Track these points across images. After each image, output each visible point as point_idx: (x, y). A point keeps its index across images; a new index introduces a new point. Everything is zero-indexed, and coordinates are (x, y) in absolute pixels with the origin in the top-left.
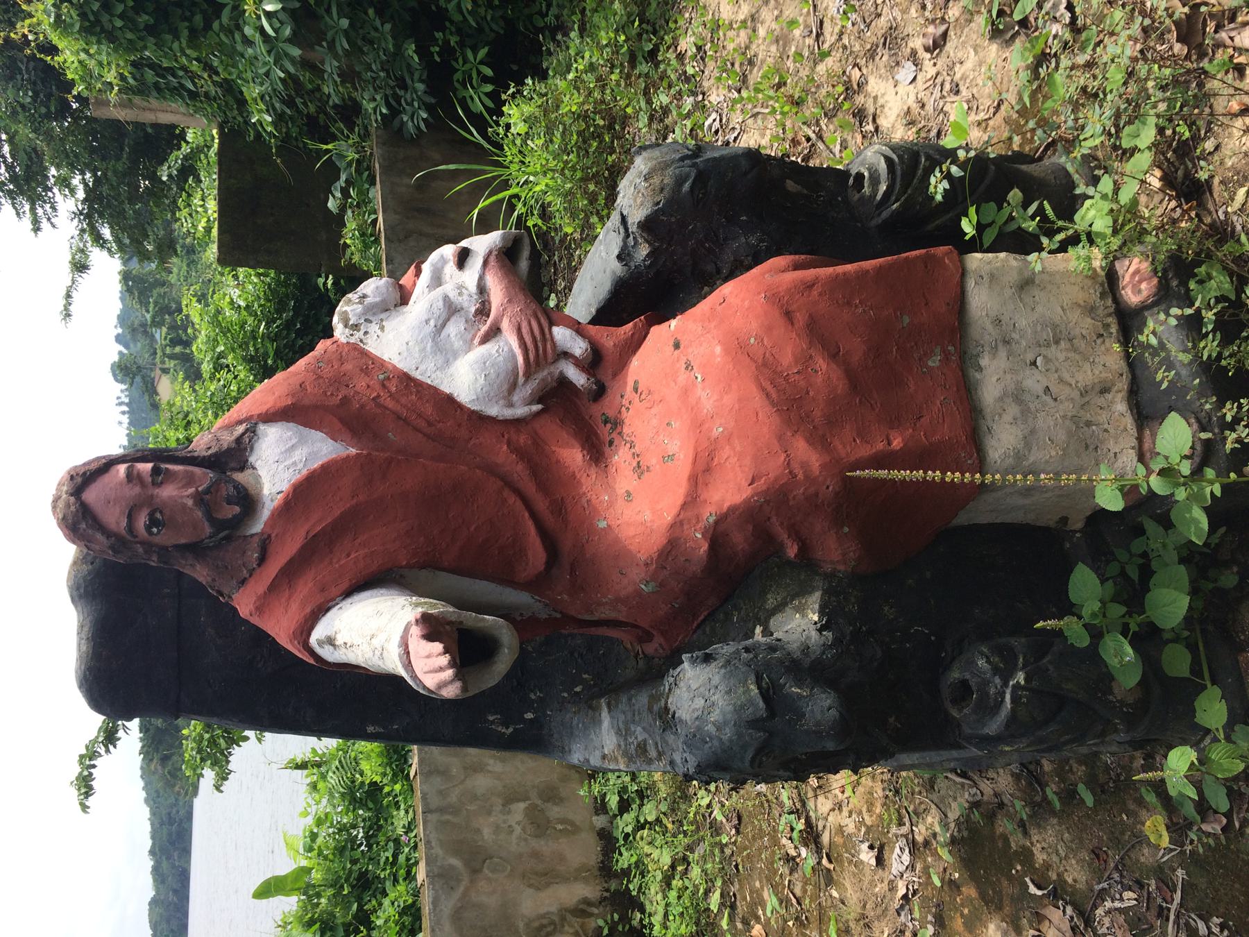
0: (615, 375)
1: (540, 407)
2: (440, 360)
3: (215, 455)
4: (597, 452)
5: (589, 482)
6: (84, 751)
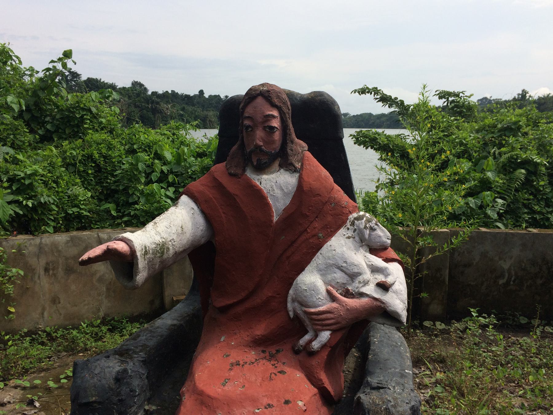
0: (300, 361)
1: (292, 316)
2: (321, 267)
3: (287, 153)
5: (245, 336)
6: (378, 89)
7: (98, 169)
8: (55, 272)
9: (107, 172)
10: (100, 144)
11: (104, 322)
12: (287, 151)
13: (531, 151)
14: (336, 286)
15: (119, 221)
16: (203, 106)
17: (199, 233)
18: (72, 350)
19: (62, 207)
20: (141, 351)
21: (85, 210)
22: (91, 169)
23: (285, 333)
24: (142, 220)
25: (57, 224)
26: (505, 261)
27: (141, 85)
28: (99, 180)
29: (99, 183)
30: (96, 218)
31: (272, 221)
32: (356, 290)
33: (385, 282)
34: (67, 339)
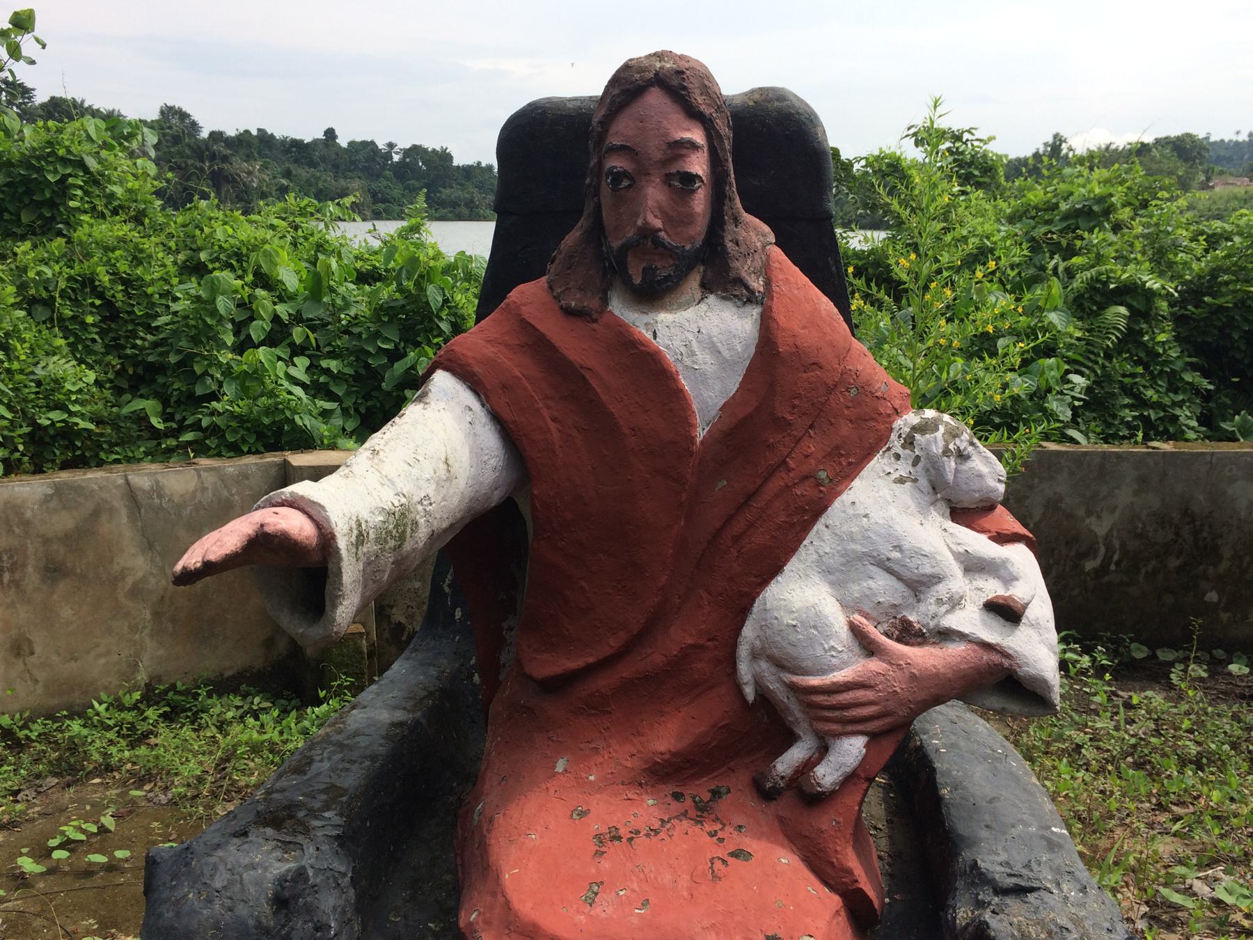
0: (781, 820)
4: (667, 774)
5: (622, 755)
7: (110, 312)
8: (17, 576)
9: (132, 321)
10: (113, 251)
11: (150, 696)
12: (723, 245)
13: (1138, 262)
14: (874, 614)
15: (171, 442)
16: (336, 167)
17: (489, 477)
18: (73, 770)
19: (22, 410)
20: (327, 807)
21: (82, 416)
22: (91, 313)
23: (739, 745)
24: (230, 438)
25: (12, 453)
26: (1099, 517)
27: (183, 116)
28: (114, 339)
29: (114, 347)
30: (109, 435)
31: (692, 439)
32: (932, 624)
33: (1010, 597)
34: (56, 742)
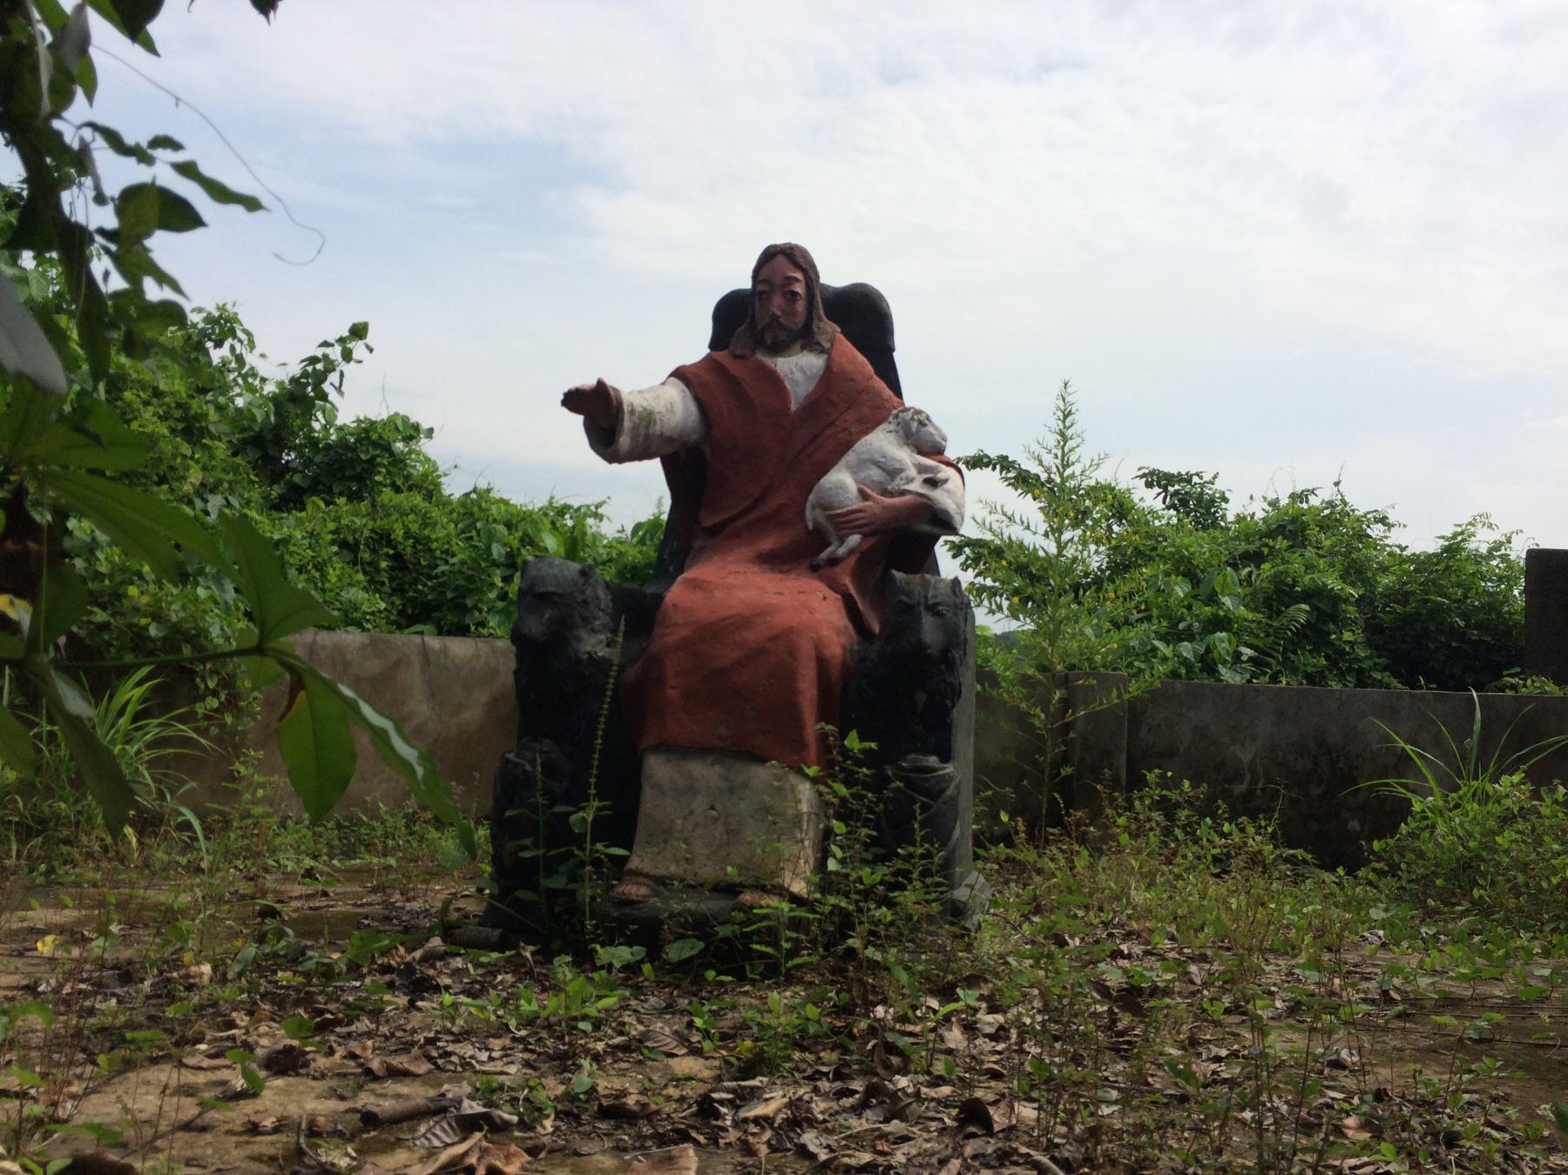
5: (747, 552)
